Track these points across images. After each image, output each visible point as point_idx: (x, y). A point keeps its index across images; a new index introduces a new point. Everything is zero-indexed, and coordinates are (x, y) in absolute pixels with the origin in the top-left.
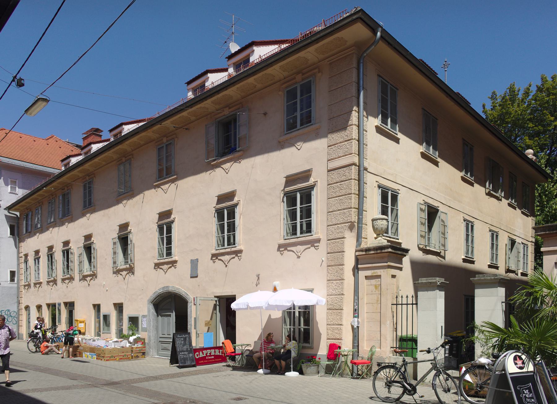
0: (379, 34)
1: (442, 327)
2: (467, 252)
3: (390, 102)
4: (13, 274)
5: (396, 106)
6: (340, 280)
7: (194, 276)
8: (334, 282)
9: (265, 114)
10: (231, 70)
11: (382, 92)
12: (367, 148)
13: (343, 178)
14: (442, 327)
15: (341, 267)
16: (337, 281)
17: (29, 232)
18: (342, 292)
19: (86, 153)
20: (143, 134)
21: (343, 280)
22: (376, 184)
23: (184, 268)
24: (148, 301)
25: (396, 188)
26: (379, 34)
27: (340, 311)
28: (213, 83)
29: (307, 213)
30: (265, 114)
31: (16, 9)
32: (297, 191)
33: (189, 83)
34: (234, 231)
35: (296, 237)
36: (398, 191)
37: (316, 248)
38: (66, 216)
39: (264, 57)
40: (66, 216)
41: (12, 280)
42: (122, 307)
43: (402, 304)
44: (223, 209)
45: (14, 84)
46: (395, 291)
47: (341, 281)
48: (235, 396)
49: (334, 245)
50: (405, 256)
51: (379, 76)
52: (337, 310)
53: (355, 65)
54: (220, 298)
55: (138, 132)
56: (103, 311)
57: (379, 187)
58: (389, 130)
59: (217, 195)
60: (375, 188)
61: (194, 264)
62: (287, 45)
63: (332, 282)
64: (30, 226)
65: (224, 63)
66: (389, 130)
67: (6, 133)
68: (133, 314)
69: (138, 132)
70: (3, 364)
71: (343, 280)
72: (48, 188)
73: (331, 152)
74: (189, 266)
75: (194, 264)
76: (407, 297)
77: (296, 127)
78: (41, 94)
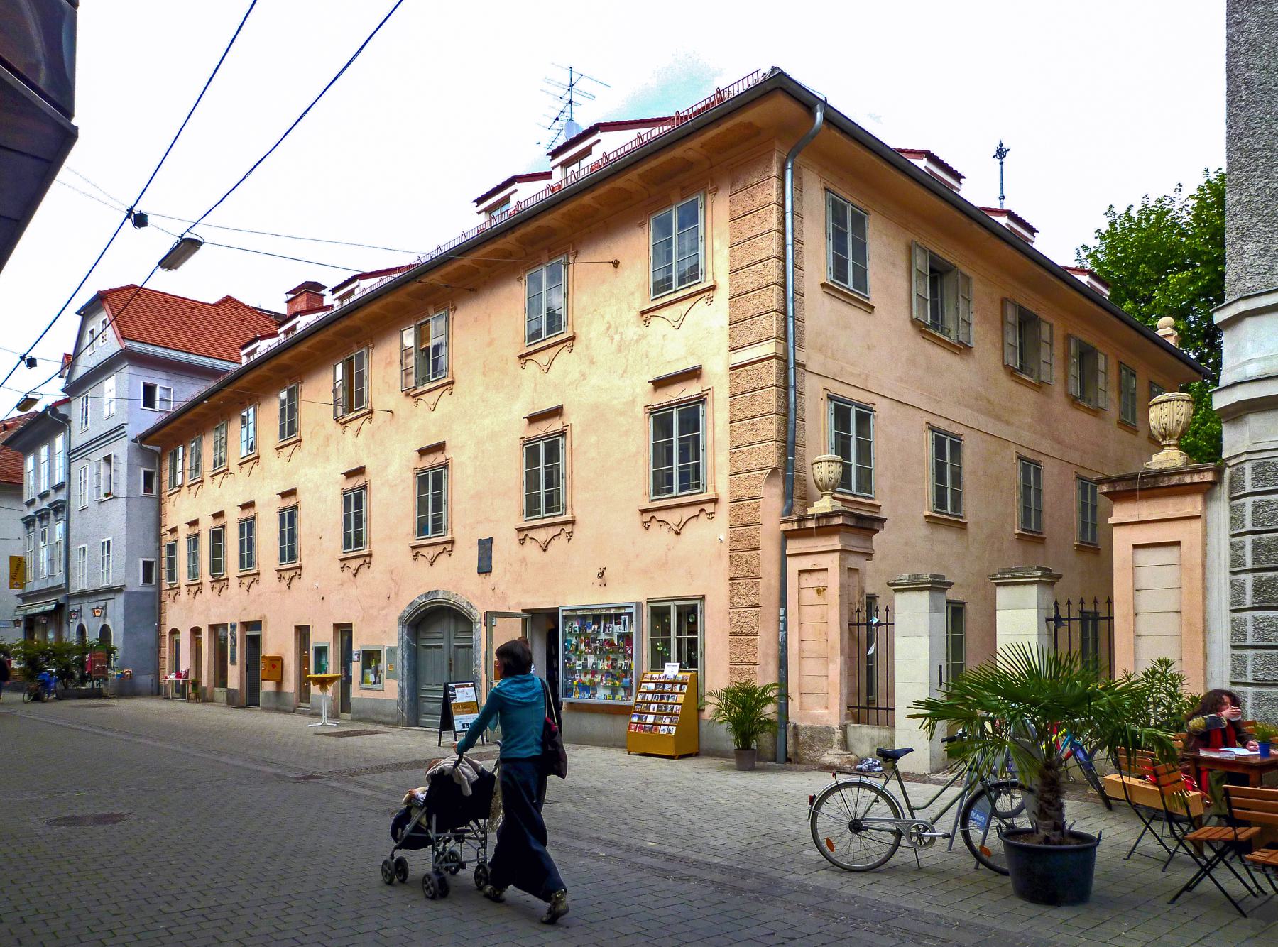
0: (819, 116)
1: (940, 667)
2: (1026, 519)
3: (853, 237)
4: (148, 566)
5: (865, 244)
6: (752, 578)
7: (485, 567)
8: (741, 581)
9: (616, 264)
10: (282, 336)
11: (835, 219)
12: (804, 327)
13: (758, 383)
14: (940, 667)
15: (754, 553)
16: (748, 581)
17: (179, 486)
18: (756, 602)
19: (286, 332)
20: (390, 299)
21: (758, 577)
22: (824, 395)
23: (467, 554)
24: (400, 618)
25: (868, 401)
26: (819, 116)
27: (752, 637)
28: (519, 204)
29: (692, 448)
30: (616, 264)
31: (31, 222)
32: (673, 408)
33: (479, 201)
34: (697, 458)
35: (698, 491)
36: (871, 406)
37: (711, 516)
38: (431, 380)
39: (611, 158)
40: (431, 380)
41: (147, 578)
42: (350, 632)
43: (1069, 619)
44: (537, 439)
45: (129, 222)
46: (857, 599)
47: (754, 580)
48: (1170, 897)
49: (741, 511)
50: (877, 531)
51: (826, 189)
52: (747, 635)
53: (775, 171)
54: (533, 614)
55: (380, 296)
56: (316, 639)
57: (831, 398)
58: (851, 291)
59: (652, 379)
60: (823, 402)
61: (485, 546)
62: (665, 128)
63: (738, 581)
64: (180, 475)
65: (546, 166)
66: (851, 291)
67: (139, 295)
68: (372, 645)
69: (380, 296)
70: (429, 793)
71: (758, 577)
72: (214, 399)
73: (735, 334)
74: (475, 552)
75: (485, 546)
76: (1069, 603)
77: (670, 287)
78: (188, 231)
